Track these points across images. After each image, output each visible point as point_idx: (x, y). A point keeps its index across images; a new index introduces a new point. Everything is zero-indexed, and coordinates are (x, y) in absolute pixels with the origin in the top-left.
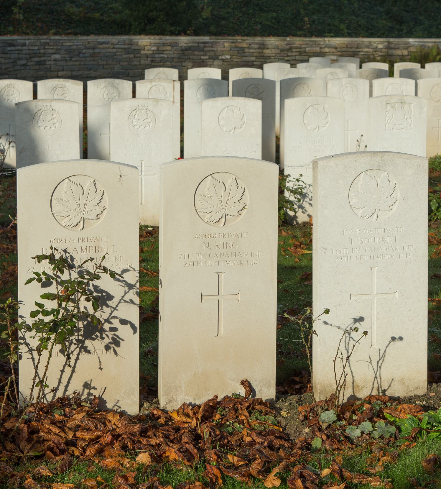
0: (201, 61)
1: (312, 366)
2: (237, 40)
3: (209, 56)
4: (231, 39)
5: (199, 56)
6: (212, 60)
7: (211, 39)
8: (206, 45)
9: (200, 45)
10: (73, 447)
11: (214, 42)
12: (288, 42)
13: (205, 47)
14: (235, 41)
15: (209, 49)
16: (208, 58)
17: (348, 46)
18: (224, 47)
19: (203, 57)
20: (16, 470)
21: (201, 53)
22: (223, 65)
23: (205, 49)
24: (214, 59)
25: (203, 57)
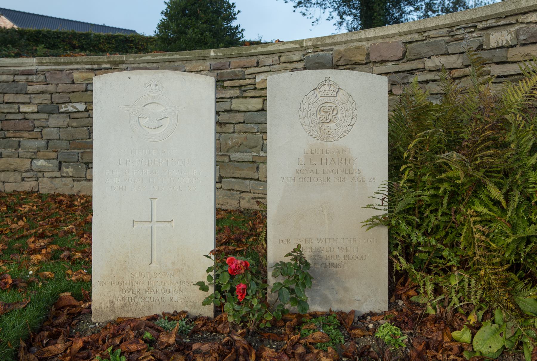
0: (20, 116)
1: (344, 69)
2: (99, 63)
3: (38, 104)
4: (86, 63)
5: (16, 106)
6: (45, 116)
7: (41, 64)
8: (31, 78)
9: (17, 78)
10: (286, 262)
11: (48, 71)
12: (213, 62)
13: (30, 83)
14: (96, 66)
15: (37, 88)
16: (34, 108)
17: (372, 58)
18: (73, 82)
19: (24, 109)
20: (481, 41)
21: (21, 98)
22: (70, 128)
23: (30, 88)
24: (50, 113)
25: (24, 109)
